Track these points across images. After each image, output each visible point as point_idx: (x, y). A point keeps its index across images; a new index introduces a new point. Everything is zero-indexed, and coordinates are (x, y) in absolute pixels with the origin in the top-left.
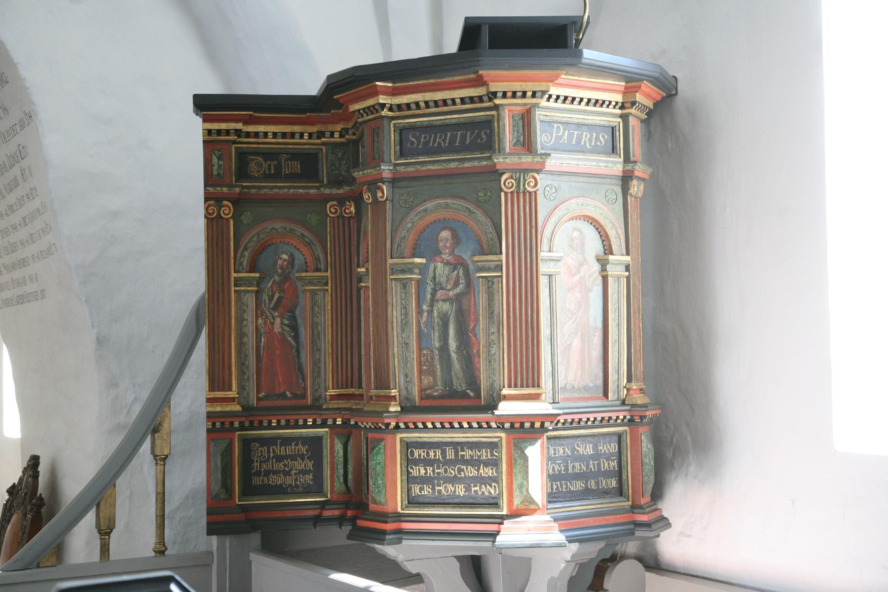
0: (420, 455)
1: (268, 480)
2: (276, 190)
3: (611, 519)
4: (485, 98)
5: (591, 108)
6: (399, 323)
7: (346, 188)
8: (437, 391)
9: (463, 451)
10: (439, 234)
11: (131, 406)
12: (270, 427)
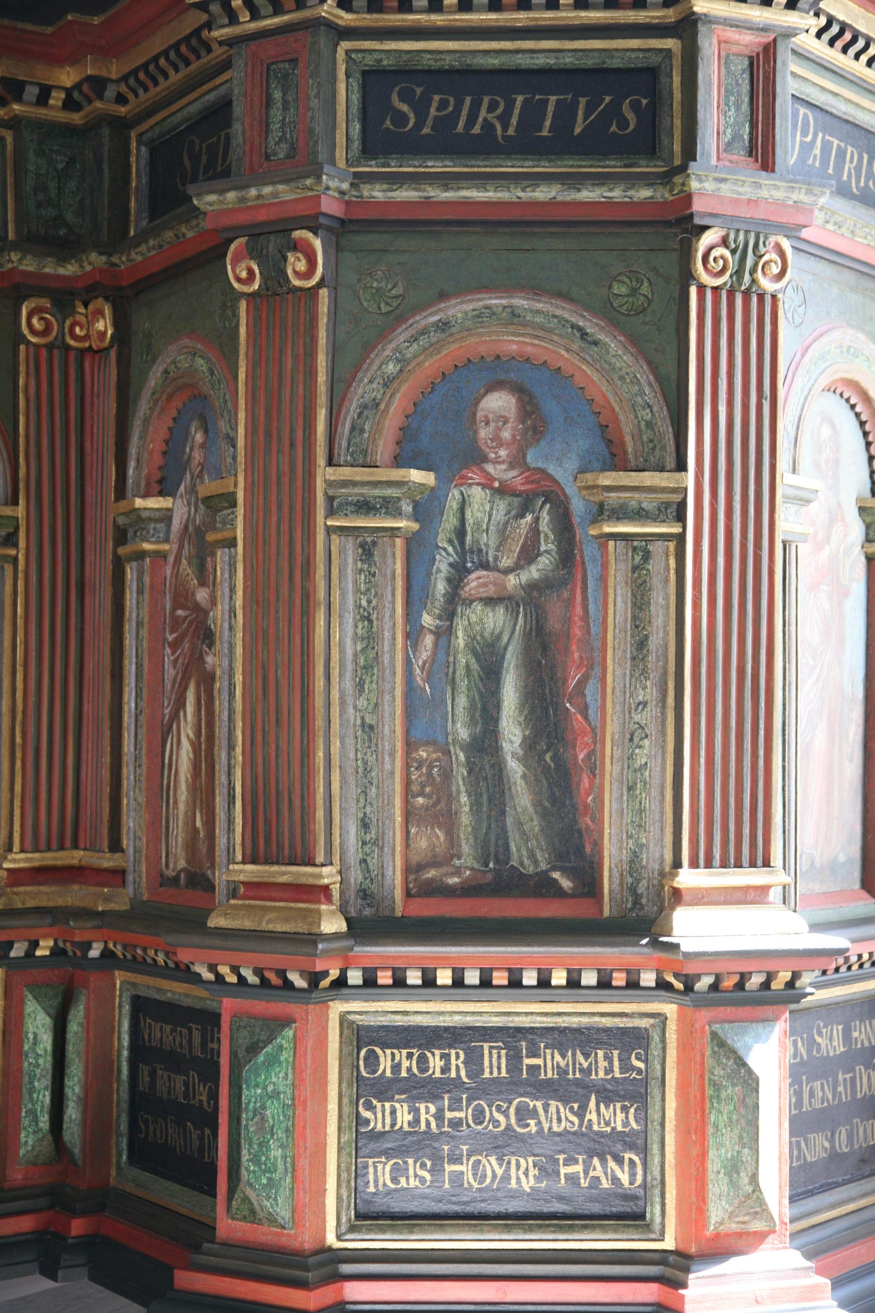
0: (396, 1068)
6: (350, 666)
7: (94, 256)
8: (458, 871)
9: (534, 1054)
10: (478, 401)
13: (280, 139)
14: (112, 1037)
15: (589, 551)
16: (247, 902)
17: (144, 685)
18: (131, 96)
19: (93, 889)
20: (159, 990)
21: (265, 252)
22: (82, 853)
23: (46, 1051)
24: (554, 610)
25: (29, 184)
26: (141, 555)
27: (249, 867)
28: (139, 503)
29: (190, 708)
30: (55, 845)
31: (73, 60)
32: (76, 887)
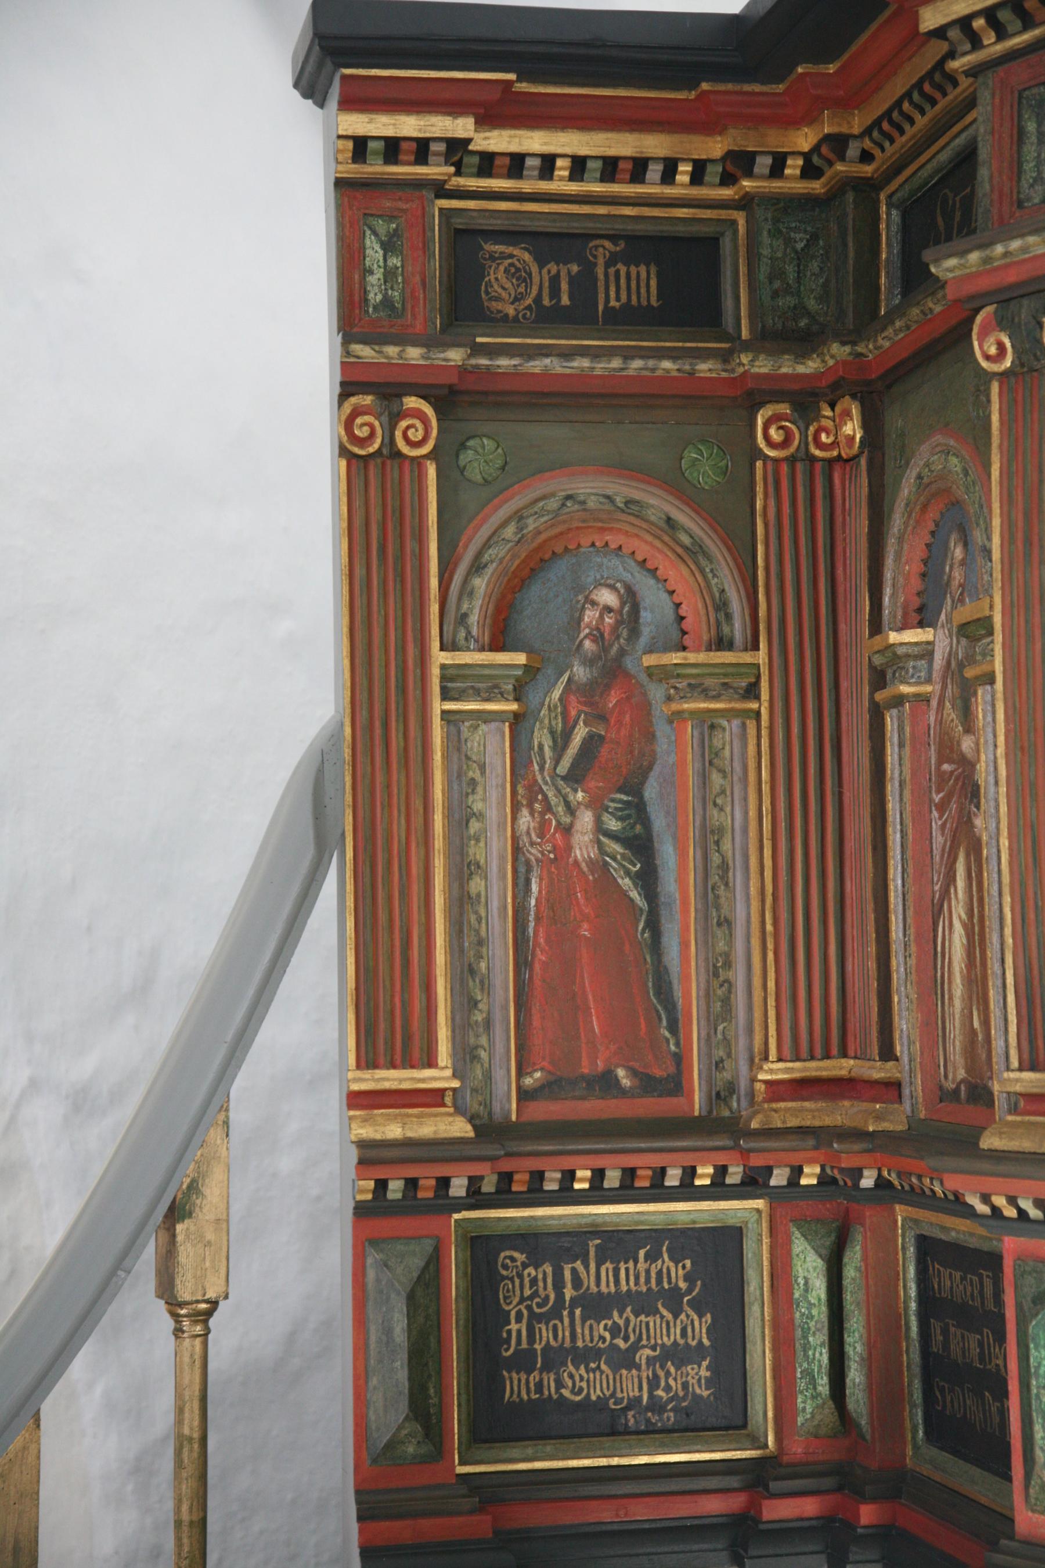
1: (559, 1384)
7: (835, 348)
11: (18, 1106)
12: (566, 1195)
13: (1035, 180)
14: (897, 1285)
16: (1027, 1118)
17: (909, 853)
18: (877, 152)
19: (865, 1105)
20: (943, 1228)
21: (1016, 320)
22: (852, 1062)
23: (820, 1300)
25: (763, 271)
26: (899, 700)
27: (1027, 1075)
28: (894, 637)
29: (961, 883)
30: (818, 1051)
31: (810, 118)
32: (847, 1103)
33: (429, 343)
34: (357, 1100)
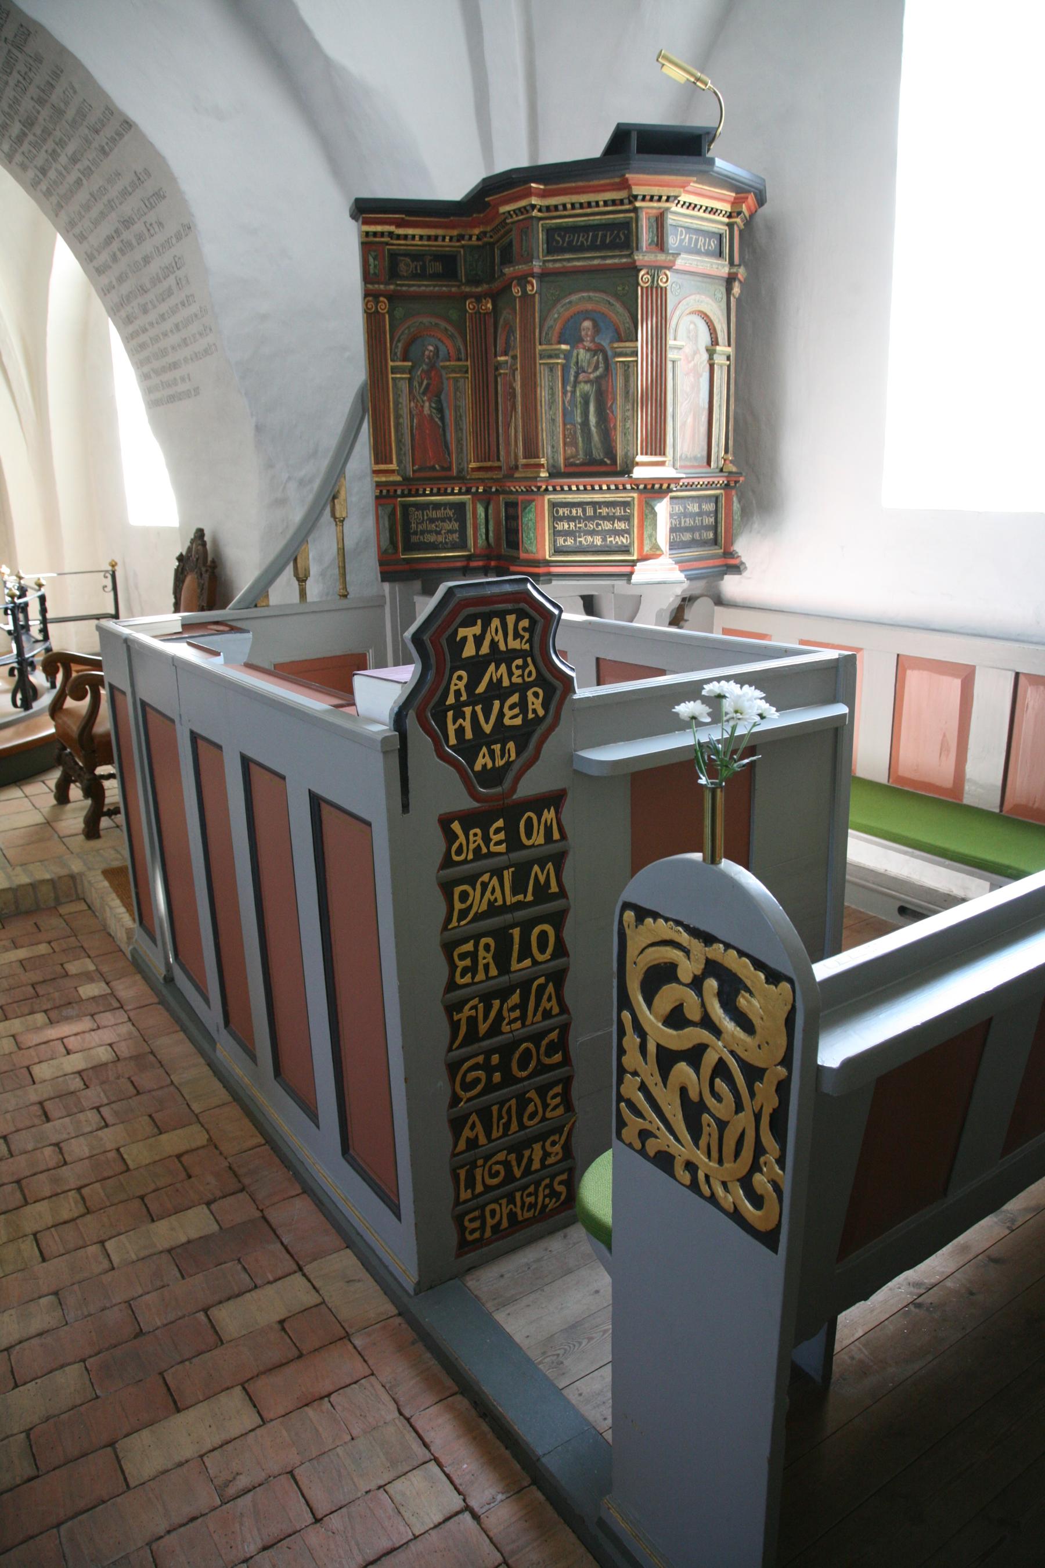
2: (423, 288)
3: (711, 563)
4: (626, 201)
5: (707, 215)
15: (613, 366)
24: (603, 382)
26: (500, 374)
33: (386, 284)
34: (375, 472)
